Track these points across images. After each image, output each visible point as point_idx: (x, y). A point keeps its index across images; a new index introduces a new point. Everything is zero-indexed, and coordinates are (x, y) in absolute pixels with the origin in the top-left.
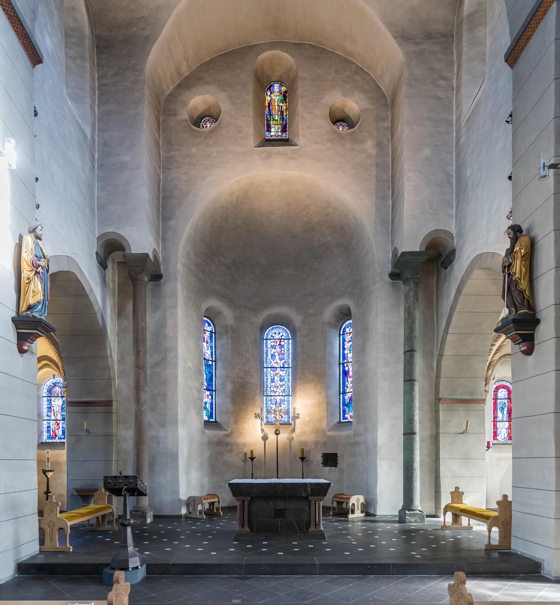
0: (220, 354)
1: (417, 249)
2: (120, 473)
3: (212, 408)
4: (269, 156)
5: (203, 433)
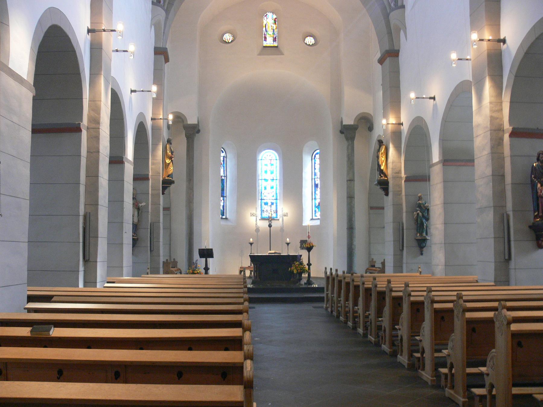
2: (309, 237)
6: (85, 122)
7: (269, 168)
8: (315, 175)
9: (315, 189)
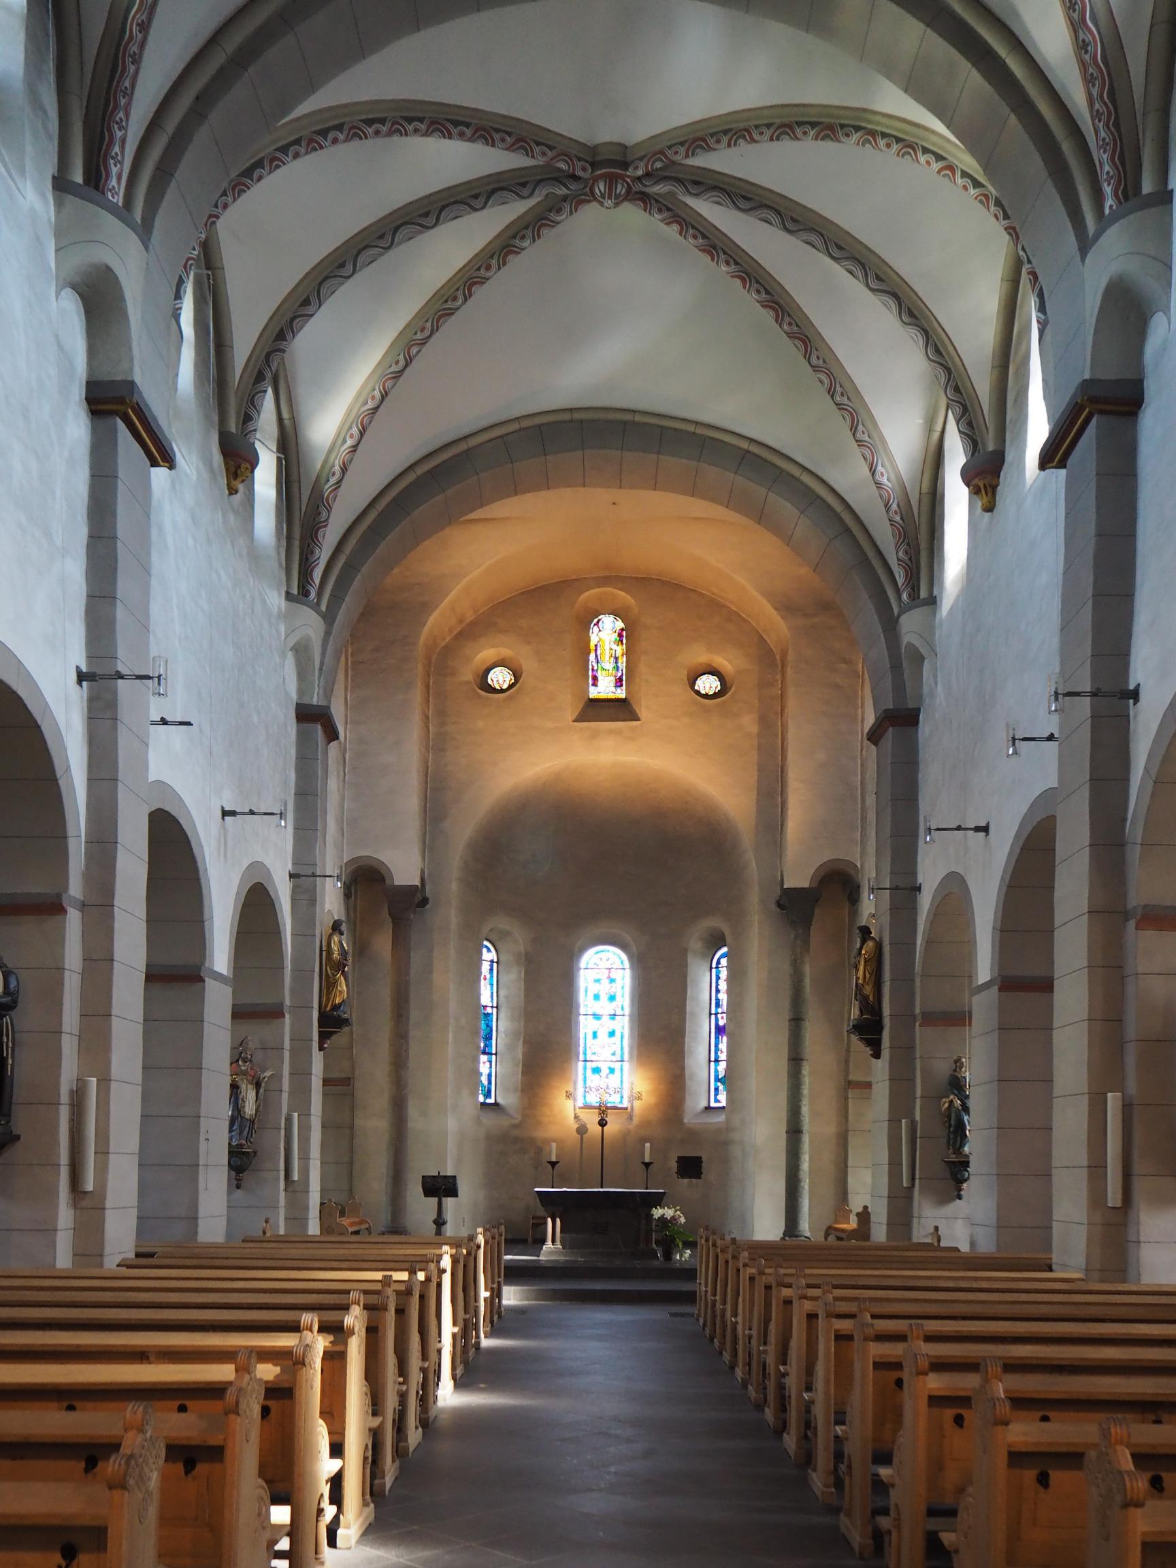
0: (506, 997)
1: (806, 885)
3: (490, 1083)
4: (595, 735)
5: (478, 1121)
6: (75, 888)
7: (604, 989)
8: (718, 1005)
9: (717, 1038)
